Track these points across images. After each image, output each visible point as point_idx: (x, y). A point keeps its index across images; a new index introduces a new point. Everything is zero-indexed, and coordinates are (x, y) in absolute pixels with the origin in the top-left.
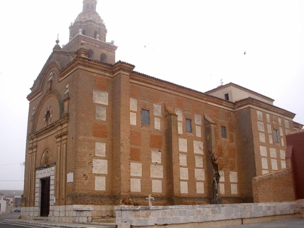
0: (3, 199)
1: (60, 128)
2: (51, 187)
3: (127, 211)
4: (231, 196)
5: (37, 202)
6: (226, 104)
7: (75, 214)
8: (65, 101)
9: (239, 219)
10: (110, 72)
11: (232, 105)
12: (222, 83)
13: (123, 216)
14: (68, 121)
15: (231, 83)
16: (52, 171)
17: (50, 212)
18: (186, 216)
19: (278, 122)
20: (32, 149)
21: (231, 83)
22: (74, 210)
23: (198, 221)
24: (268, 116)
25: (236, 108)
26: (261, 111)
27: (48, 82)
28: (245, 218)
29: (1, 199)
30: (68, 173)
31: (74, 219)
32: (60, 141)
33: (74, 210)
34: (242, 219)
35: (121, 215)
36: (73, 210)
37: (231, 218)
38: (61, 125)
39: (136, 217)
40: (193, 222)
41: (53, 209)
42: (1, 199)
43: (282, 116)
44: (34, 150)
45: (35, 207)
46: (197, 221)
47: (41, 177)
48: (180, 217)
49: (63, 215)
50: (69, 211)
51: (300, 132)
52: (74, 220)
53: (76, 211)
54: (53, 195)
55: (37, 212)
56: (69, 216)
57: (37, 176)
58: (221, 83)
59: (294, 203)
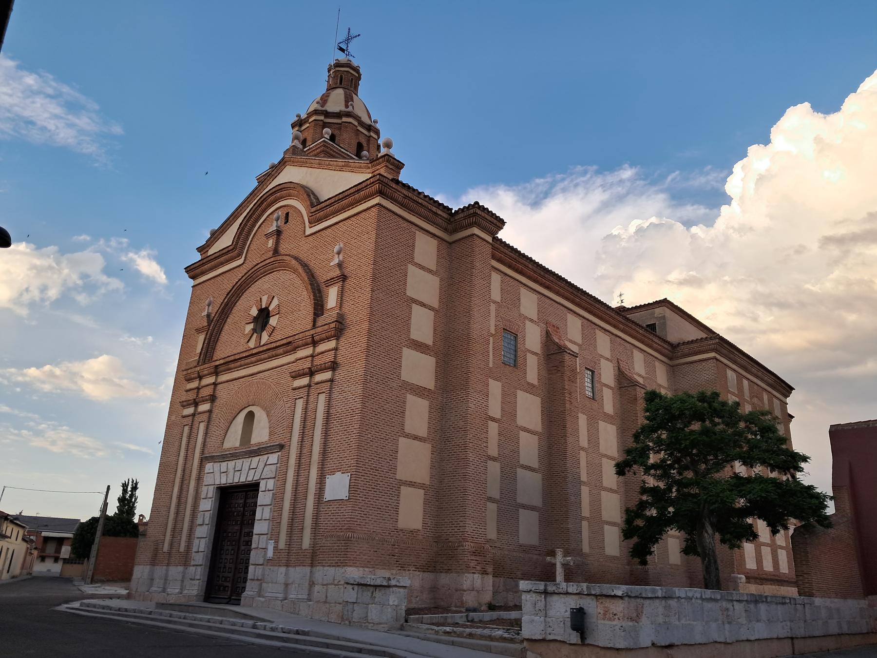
0: (21, 538)
1: (308, 351)
2: (259, 511)
3: (568, 596)
4: (168, 584)
5: (200, 553)
6: (659, 345)
7: (351, 595)
8: (330, 282)
9: (788, 638)
10: (445, 230)
11: (670, 348)
12: (622, 302)
13: (551, 613)
14: (339, 333)
15: (666, 299)
16: (241, 470)
17: (249, 584)
18: (703, 621)
19: (762, 400)
20: (196, 404)
21: (666, 299)
22: (348, 583)
23: (726, 639)
24: (745, 382)
25: (678, 358)
26: (734, 370)
27: (268, 236)
28: (797, 638)
29: (16, 540)
30: (333, 473)
31: (348, 611)
32: (330, 381)
33: (348, 583)
34: (792, 638)
35: (546, 607)
36: (342, 582)
37: (746, 639)
38: (315, 343)
39: (610, 619)
40: (716, 642)
41: (263, 575)
42: (16, 540)
43: (769, 389)
44: (204, 407)
45: (192, 569)
46: (722, 640)
47: (224, 481)
48: (695, 623)
49: (300, 597)
50: (327, 585)
51: (868, 426)
52: (346, 613)
53: (356, 587)
54: (265, 536)
55: (198, 582)
56: (325, 602)
57: (207, 479)
58: (620, 302)
59: (863, 603)
